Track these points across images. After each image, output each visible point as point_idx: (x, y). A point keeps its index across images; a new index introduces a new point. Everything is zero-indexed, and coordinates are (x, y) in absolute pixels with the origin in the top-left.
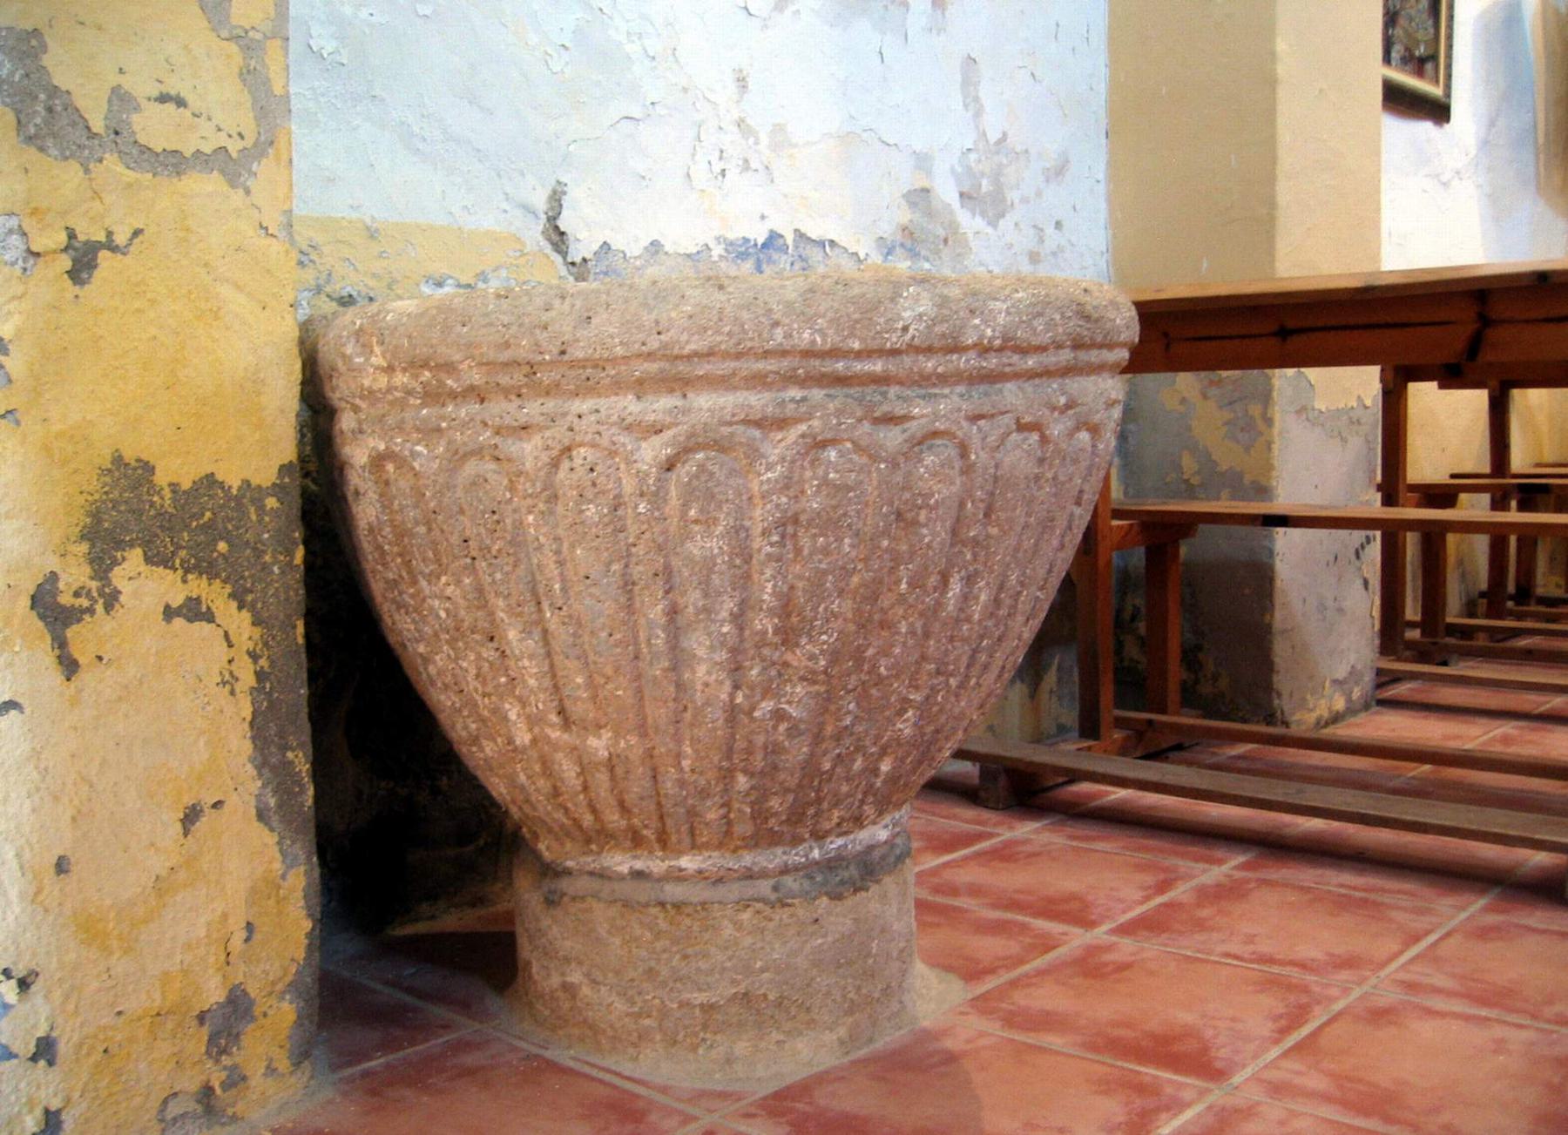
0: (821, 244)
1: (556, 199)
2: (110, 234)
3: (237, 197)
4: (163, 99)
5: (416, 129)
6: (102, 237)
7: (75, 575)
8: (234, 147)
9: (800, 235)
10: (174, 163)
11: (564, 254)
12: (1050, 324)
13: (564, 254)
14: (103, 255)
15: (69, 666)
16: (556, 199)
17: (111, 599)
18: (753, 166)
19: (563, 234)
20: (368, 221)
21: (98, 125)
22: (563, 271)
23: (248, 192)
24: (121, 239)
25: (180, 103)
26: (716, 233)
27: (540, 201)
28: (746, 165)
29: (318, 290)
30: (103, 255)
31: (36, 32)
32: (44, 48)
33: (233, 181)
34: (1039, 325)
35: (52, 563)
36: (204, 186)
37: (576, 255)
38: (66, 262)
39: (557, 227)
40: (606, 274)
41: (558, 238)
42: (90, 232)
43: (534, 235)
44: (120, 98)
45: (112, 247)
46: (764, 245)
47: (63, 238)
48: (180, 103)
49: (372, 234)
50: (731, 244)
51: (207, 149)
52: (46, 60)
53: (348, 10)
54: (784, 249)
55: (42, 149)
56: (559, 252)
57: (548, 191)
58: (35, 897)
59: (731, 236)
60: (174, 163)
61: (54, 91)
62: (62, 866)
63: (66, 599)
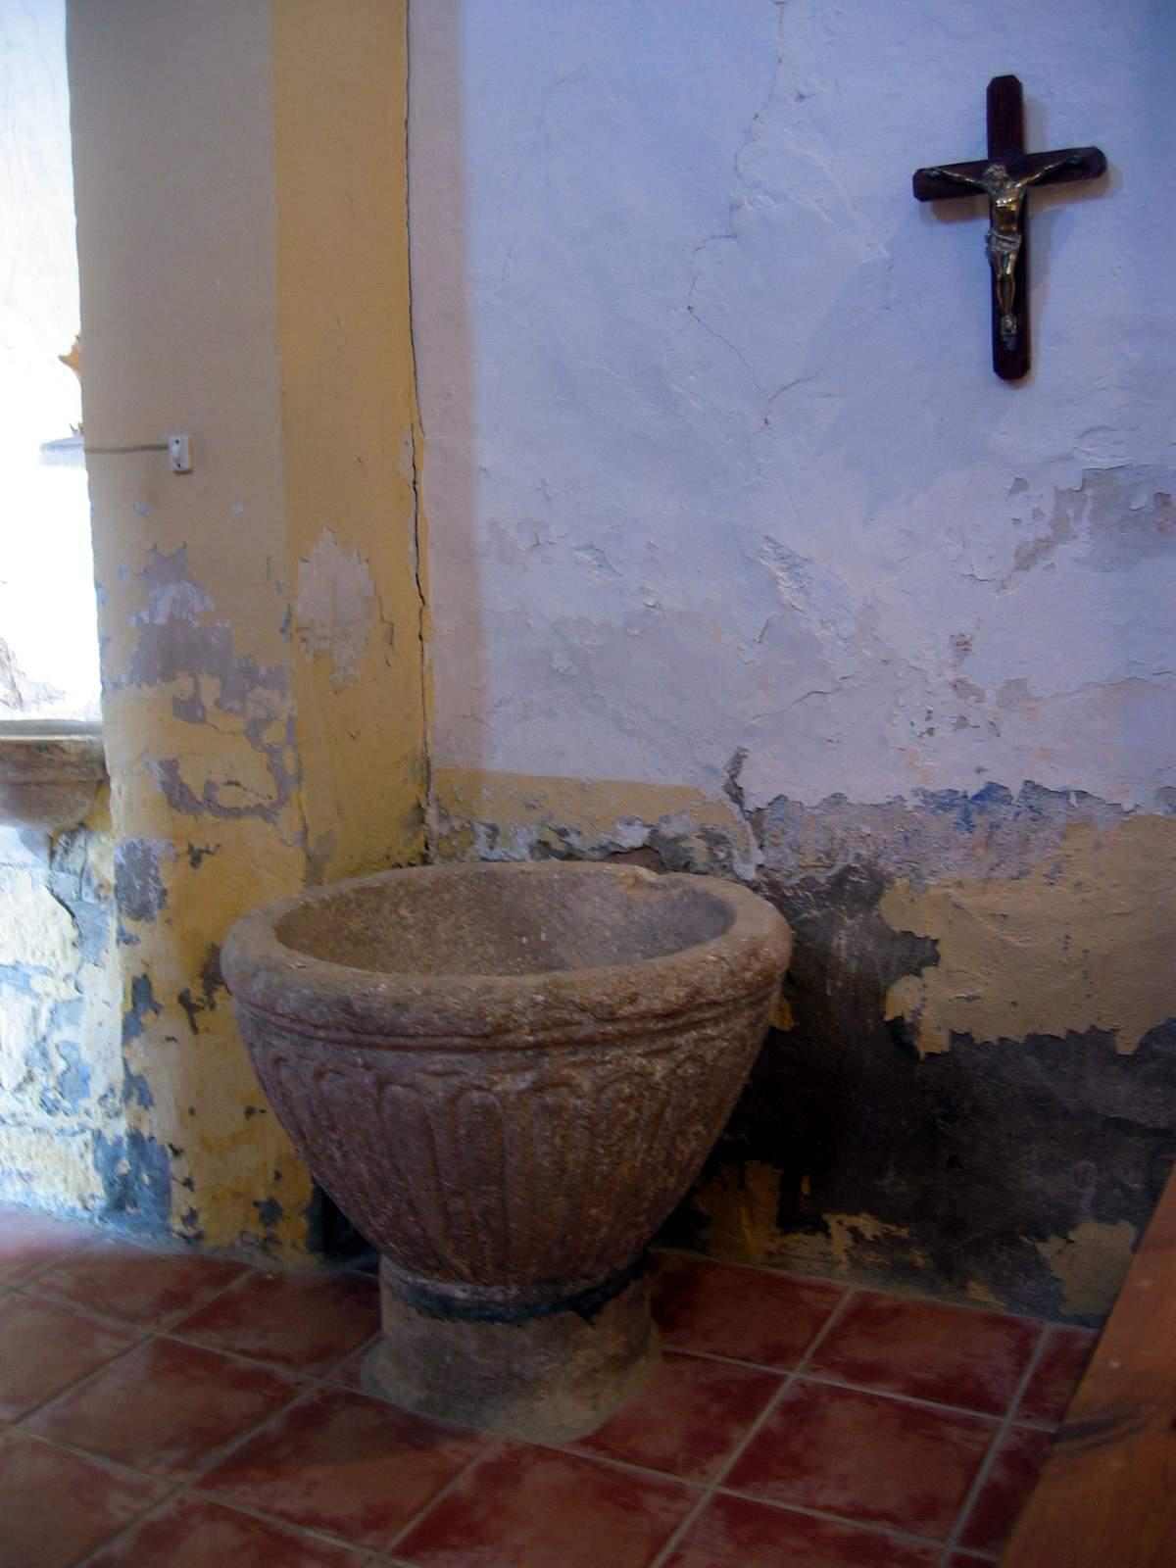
0: (1064, 794)
1: (738, 761)
2: (207, 847)
3: (270, 827)
4: (230, 783)
5: (625, 715)
6: (203, 848)
7: (197, 993)
8: (266, 803)
9: (1032, 787)
10: (236, 813)
11: (740, 803)
12: (321, 1014)
13: (740, 803)
14: (205, 855)
15: (195, 1029)
16: (738, 761)
17: (213, 1006)
18: (972, 722)
19: (741, 788)
20: (583, 780)
21: (200, 798)
22: (739, 817)
23: (275, 824)
24: (211, 849)
25: (237, 784)
26: (914, 786)
27: (722, 759)
28: (962, 722)
29: (543, 824)
30: (205, 855)
31: (175, 761)
32: (178, 767)
33: (267, 819)
34: (314, 1013)
35: (187, 985)
36: (252, 823)
37: (751, 804)
38: (189, 858)
39: (735, 784)
40: (781, 820)
41: (736, 795)
42: (198, 846)
43: (715, 789)
44: (210, 786)
45: (208, 852)
46: (976, 797)
47: (186, 848)
48: (237, 784)
49: (583, 788)
50: (933, 795)
51: (252, 805)
52: (179, 772)
53: (577, 641)
54: (1007, 800)
55: (179, 810)
56: (736, 802)
57: (732, 754)
58: (181, 1120)
59: (932, 788)
60: (236, 813)
61: (182, 785)
62: (192, 1112)
63: (194, 1001)
